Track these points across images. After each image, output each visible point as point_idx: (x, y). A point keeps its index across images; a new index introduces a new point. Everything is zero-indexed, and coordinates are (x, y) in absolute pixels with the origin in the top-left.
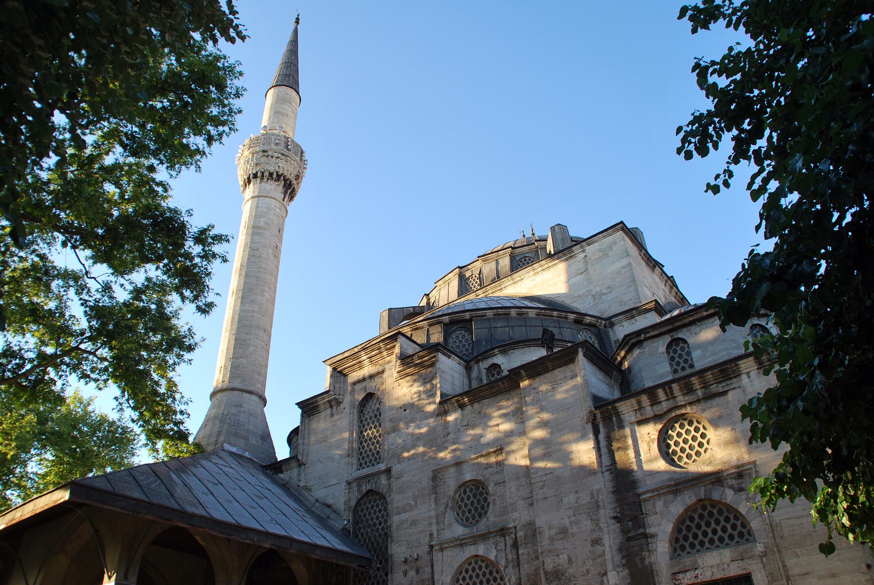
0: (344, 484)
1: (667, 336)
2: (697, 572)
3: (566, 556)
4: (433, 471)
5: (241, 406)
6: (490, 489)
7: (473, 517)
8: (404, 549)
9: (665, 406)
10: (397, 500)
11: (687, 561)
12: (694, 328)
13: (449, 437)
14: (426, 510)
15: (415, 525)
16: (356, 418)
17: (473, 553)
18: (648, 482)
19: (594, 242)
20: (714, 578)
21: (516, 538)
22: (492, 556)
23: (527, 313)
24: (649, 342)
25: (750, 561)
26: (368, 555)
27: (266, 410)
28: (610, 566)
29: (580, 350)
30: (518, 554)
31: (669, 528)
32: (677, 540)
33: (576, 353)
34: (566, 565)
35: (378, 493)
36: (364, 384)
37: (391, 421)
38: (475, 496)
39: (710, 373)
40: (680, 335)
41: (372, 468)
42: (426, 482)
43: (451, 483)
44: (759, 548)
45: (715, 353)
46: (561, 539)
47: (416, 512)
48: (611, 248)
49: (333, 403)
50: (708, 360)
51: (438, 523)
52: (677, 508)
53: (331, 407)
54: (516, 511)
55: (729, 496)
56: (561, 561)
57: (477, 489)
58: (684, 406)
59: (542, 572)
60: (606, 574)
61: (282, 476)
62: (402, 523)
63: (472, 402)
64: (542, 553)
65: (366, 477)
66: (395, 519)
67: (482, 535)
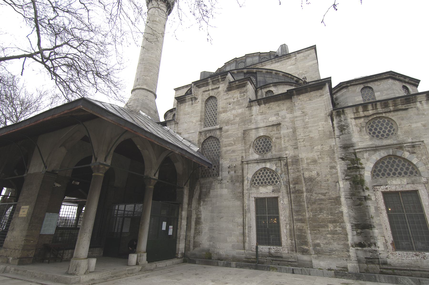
0: (198, 133)
1: (362, 85)
2: (387, 186)
3: (316, 172)
4: (244, 131)
5: (147, 97)
6: (273, 140)
7: (263, 151)
8: (228, 162)
9: (371, 112)
10: (224, 141)
11: (381, 180)
12: (376, 83)
13: (253, 117)
14: (239, 147)
15: (234, 152)
16: (204, 105)
17: (264, 166)
18: (359, 144)
19: (302, 52)
20: (396, 190)
21: (287, 162)
22: (274, 168)
23: (279, 74)
24: (352, 87)
25: (418, 185)
26: (211, 163)
27: (157, 101)
28: (340, 179)
29: (327, 84)
30: (288, 169)
31: (372, 165)
32: (375, 171)
33: (325, 85)
34: (316, 176)
35: (214, 138)
36: (209, 92)
37: (222, 108)
38: (264, 142)
39: (400, 99)
40: (369, 85)
41: (212, 127)
42: (240, 134)
43: (253, 135)
44: (424, 180)
45: (388, 94)
46: (313, 164)
47: (235, 147)
48: (308, 56)
49: (193, 99)
50: (384, 97)
51: (246, 153)
52: (376, 157)
53: (192, 100)
54: (287, 150)
55: (406, 155)
56: (313, 174)
57: (266, 139)
58: (382, 113)
59: (303, 178)
60: (338, 182)
61: (166, 127)
62: (227, 151)
63: (265, 103)
64: (302, 170)
65: (210, 131)
66: (224, 149)
67: (269, 159)
